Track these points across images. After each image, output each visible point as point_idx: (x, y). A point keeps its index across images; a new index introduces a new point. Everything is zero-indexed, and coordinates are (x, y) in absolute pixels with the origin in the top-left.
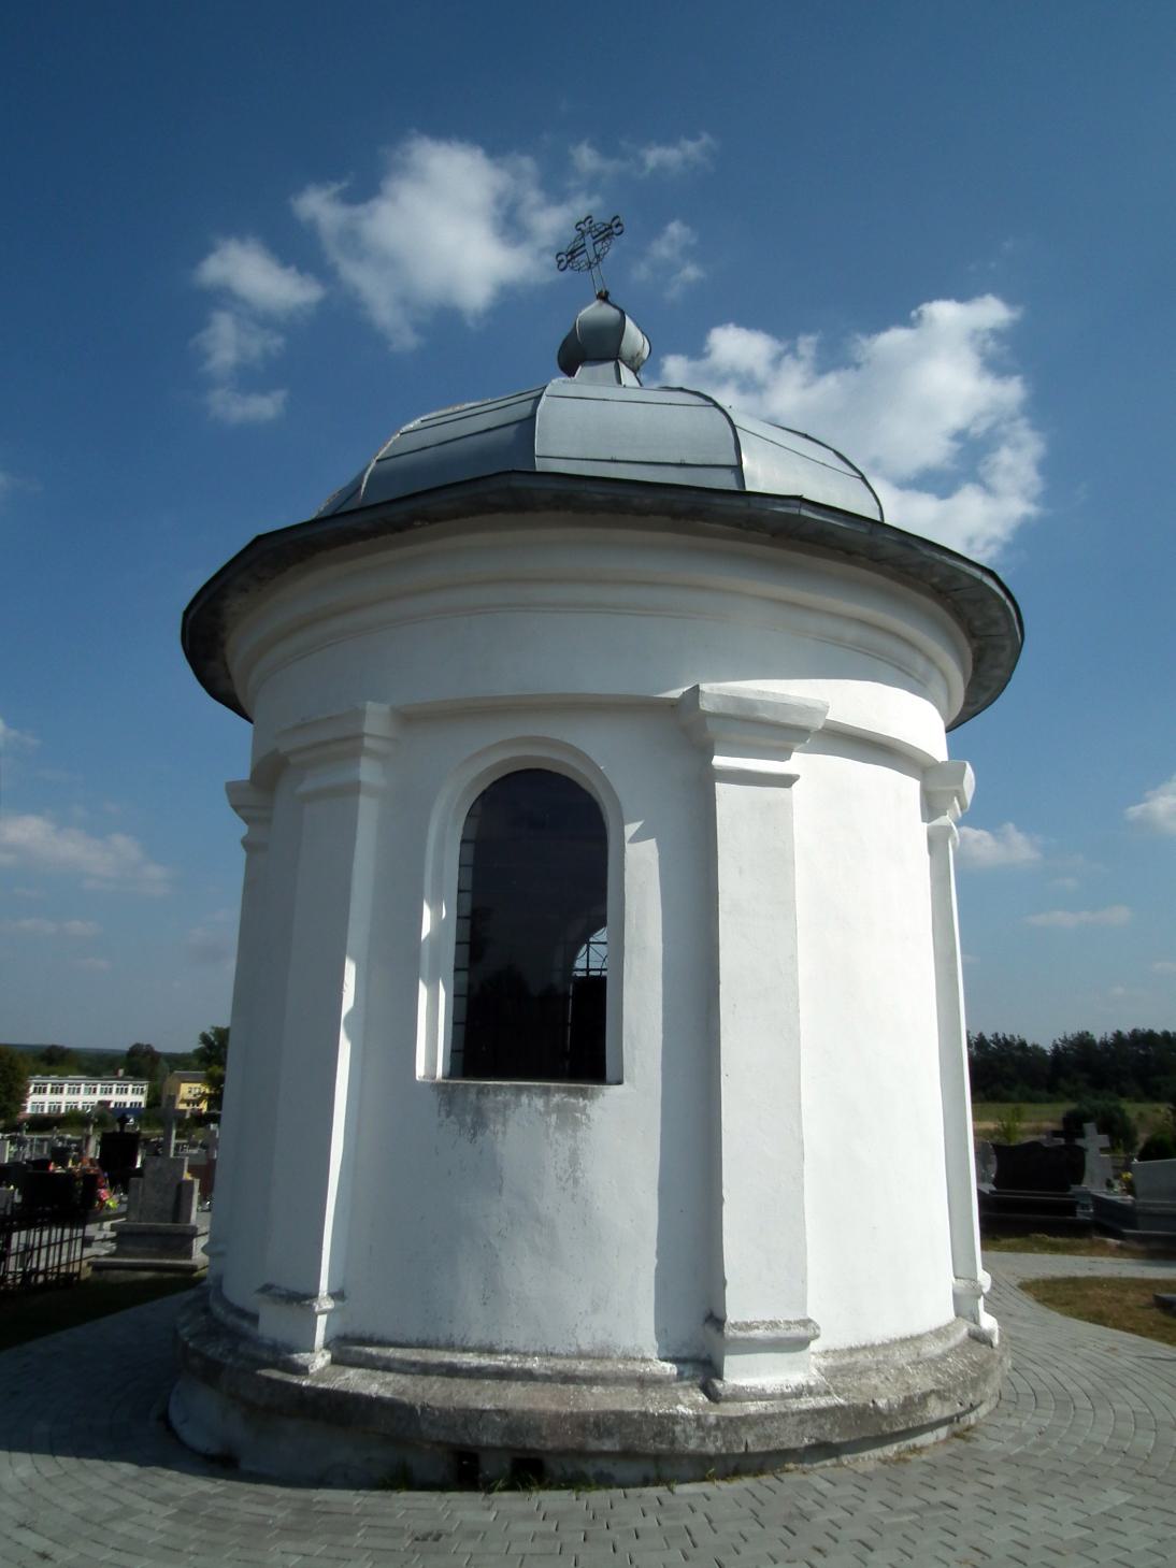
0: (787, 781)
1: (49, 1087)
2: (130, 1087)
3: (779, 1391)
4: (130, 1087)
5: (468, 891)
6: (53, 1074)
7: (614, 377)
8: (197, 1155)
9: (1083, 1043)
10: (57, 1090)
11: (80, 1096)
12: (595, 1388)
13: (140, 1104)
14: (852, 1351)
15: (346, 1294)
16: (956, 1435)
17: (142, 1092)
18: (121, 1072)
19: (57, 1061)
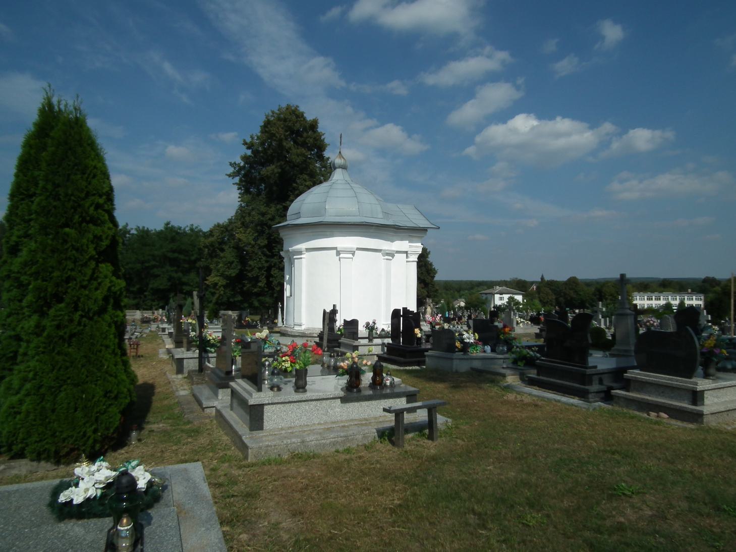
0: (301, 258)
1: (654, 297)
2: (694, 297)
3: (293, 108)
4: (694, 297)
5: (415, 261)
6: (656, 292)
7: (300, 260)
8: (294, 256)
9: (431, 264)
10: (650, 299)
11: (657, 302)
12: (104, 463)
13: (701, 305)
14: (545, 392)
15: (281, 390)
16: (315, 354)
17: (701, 299)
18: (690, 290)
19: (645, 286)
